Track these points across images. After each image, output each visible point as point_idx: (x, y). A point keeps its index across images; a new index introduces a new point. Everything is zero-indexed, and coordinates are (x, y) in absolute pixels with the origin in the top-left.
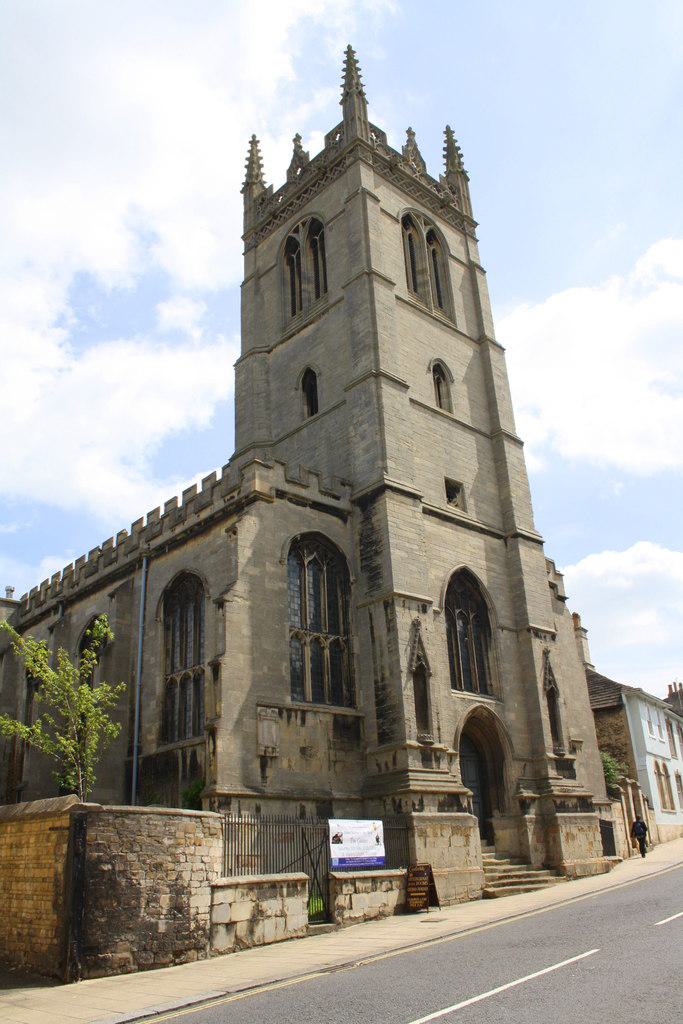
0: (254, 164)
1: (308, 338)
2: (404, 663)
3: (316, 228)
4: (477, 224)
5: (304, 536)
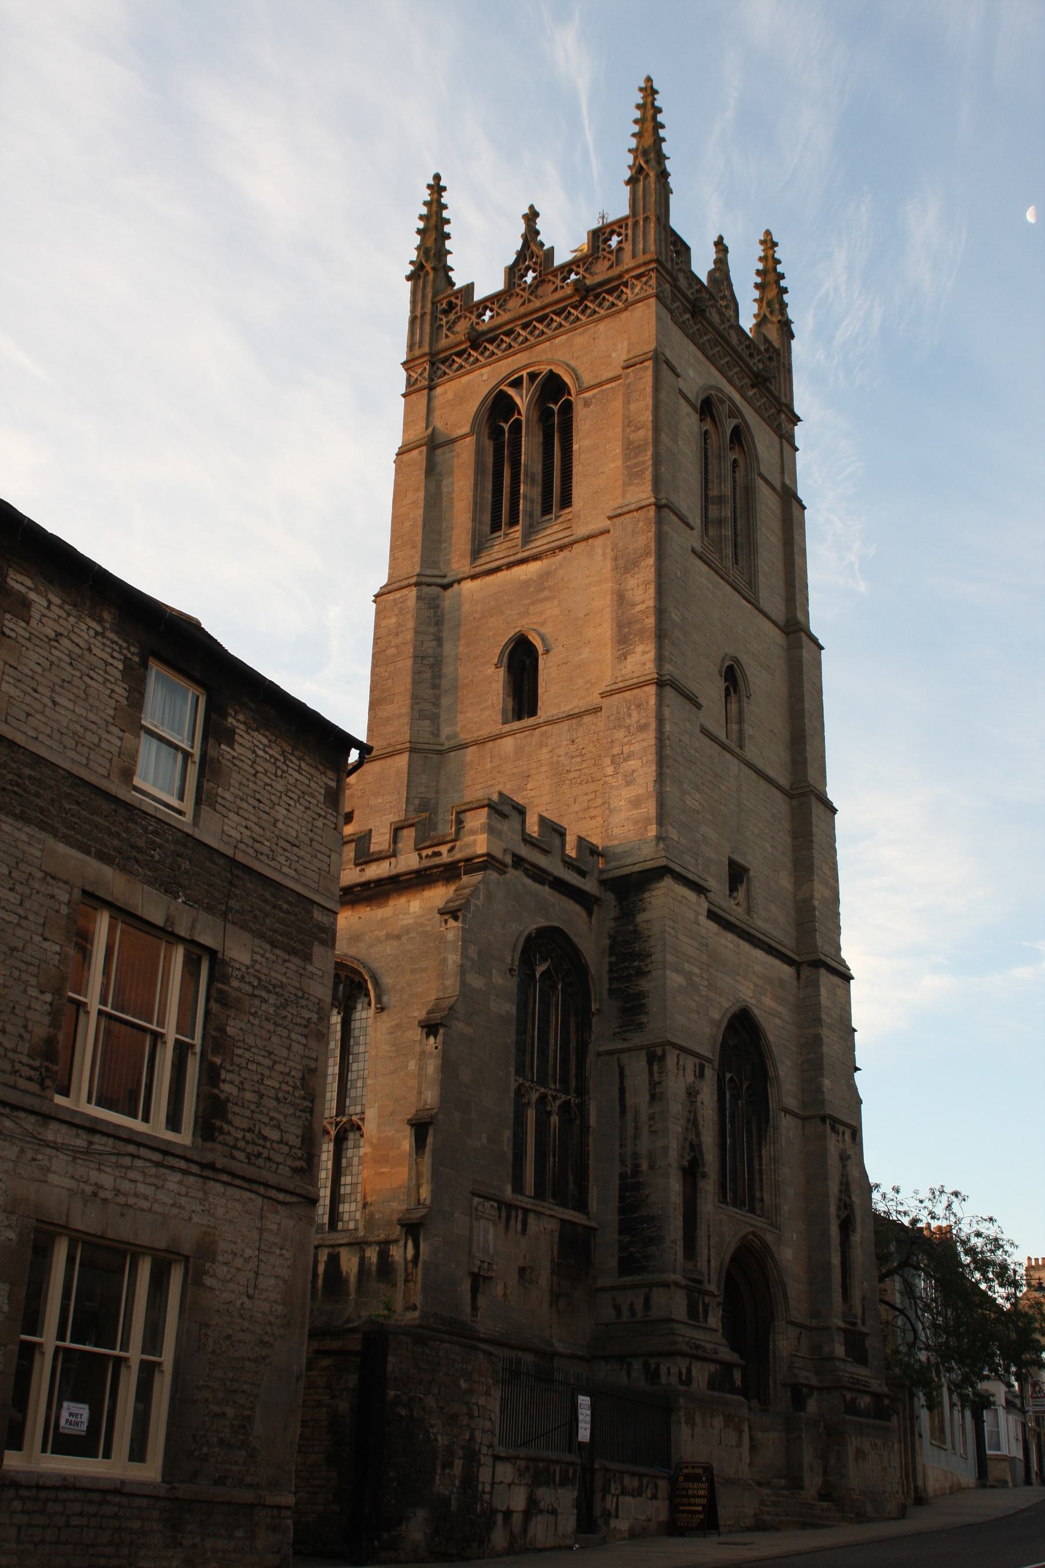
0: (434, 230)
1: (527, 583)
2: (673, 1154)
4: (799, 420)
5: (541, 931)
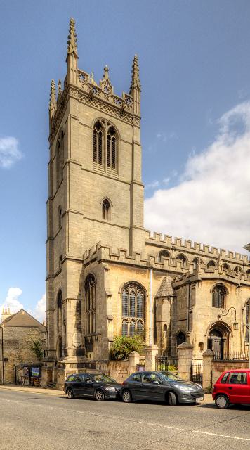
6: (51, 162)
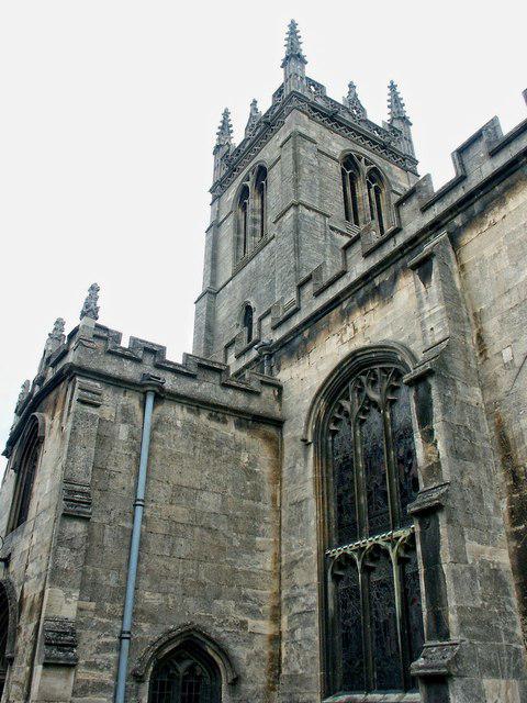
0: (225, 128)
3: (262, 172)
6: (215, 226)
